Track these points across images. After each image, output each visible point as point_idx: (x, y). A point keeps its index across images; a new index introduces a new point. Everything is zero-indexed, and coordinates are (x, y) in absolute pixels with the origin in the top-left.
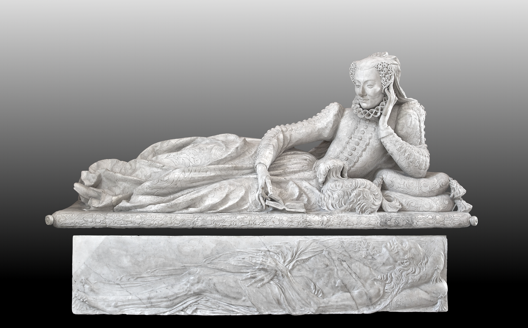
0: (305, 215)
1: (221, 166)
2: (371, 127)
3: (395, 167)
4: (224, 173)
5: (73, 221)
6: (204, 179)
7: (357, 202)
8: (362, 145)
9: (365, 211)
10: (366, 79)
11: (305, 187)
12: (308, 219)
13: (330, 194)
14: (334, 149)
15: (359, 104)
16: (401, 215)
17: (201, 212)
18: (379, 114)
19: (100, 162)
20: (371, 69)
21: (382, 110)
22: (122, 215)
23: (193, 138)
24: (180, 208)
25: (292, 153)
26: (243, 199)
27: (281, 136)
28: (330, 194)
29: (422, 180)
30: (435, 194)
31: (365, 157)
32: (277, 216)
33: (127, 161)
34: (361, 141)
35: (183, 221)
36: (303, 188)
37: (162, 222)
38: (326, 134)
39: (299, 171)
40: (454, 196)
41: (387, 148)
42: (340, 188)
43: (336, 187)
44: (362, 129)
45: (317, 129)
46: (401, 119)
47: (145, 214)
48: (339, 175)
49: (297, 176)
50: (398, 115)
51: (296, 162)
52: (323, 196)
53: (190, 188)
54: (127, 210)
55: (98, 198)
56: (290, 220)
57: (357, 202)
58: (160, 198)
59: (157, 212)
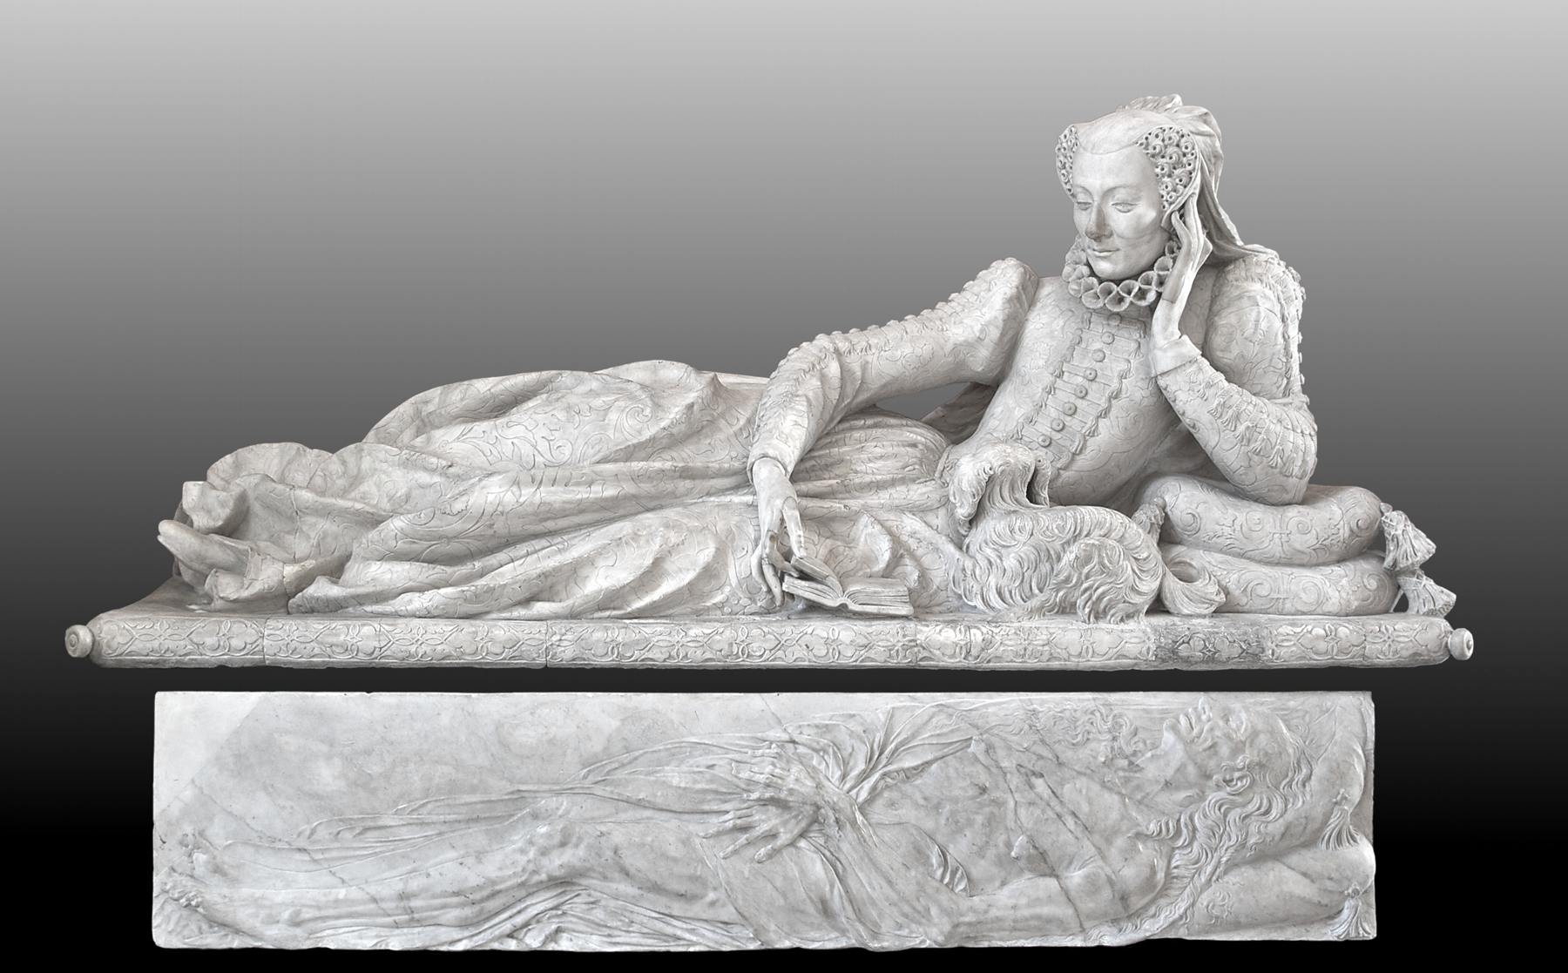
1: (636, 466)
2: (1127, 340)
4: (647, 487)
5: (156, 644)
6: (581, 508)
7: (1079, 583)
8: (1098, 397)
9: (1105, 612)
10: (1110, 182)
11: (913, 535)
12: (921, 638)
14: (1005, 409)
16: (1223, 625)
17: (574, 615)
18: (1151, 296)
19: (245, 453)
22: (316, 626)
23: (545, 374)
24: (505, 601)
25: (870, 422)
30: (1335, 557)
32: (819, 628)
33: (333, 448)
34: (1094, 386)
35: (515, 643)
36: (904, 538)
38: (980, 362)
39: (893, 483)
40: (1395, 563)
41: (1178, 407)
43: (1013, 534)
44: (1097, 345)
45: (949, 347)
46: (1224, 313)
47: (390, 621)
49: (884, 497)
51: (881, 451)
52: (968, 564)
53: (536, 536)
54: (332, 608)
55: (236, 569)
58: (439, 568)
59: (428, 615)
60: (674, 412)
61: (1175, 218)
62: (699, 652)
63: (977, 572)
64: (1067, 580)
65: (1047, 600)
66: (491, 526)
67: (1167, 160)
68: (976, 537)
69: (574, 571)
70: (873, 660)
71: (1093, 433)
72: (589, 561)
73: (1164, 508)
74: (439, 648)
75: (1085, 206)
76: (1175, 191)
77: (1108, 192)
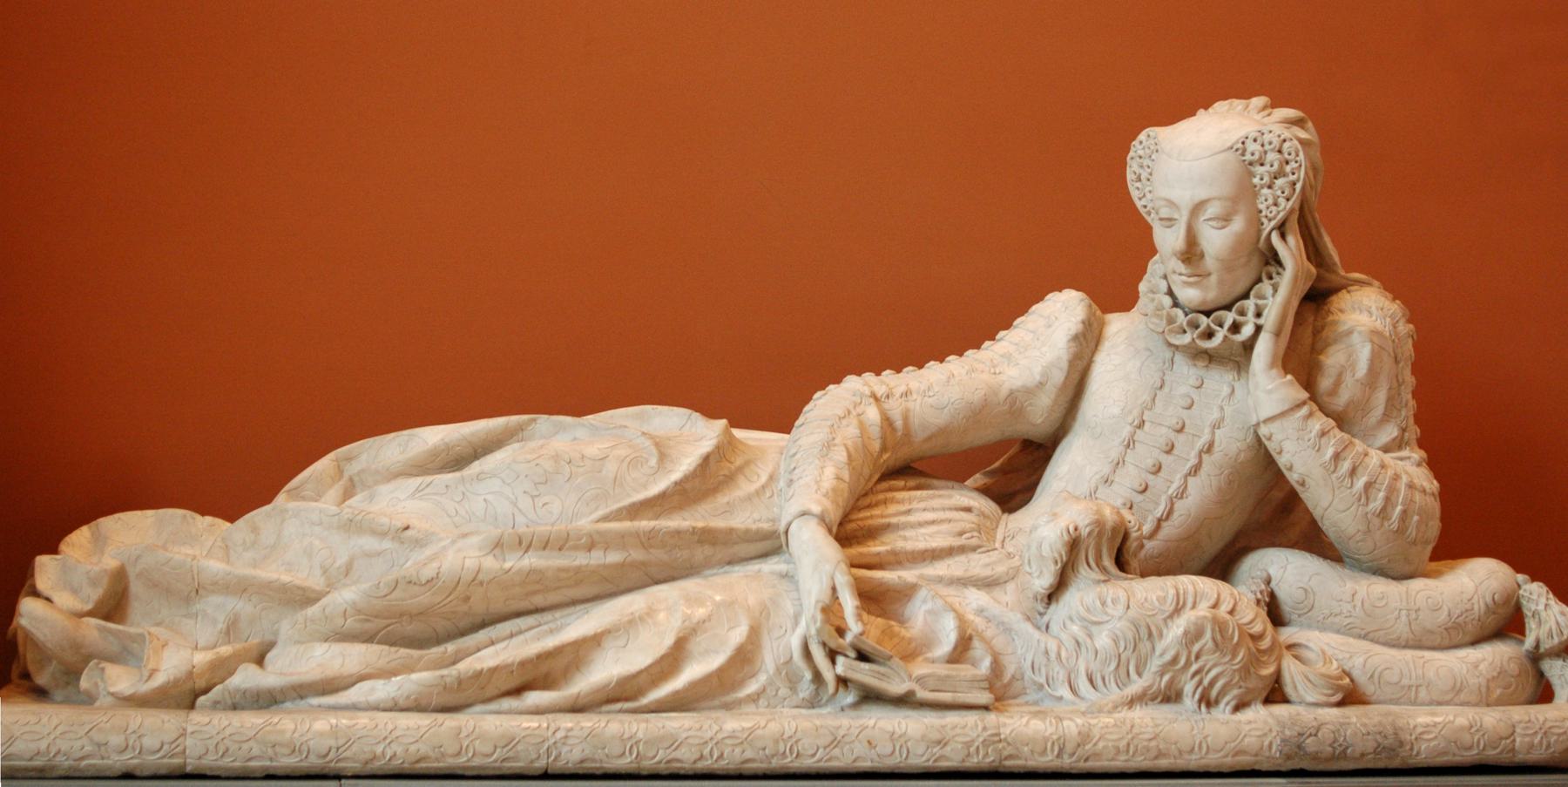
0: (991, 718)
1: (645, 524)
2: (1219, 380)
3: (1314, 541)
4: (658, 555)
5: (43, 745)
6: (578, 576)
7: (1188, 664)
8: (1187, 453)
9: (1217, 702)
10: (1202, 194)
11: (980, 611)
12: (1005, 732)
13: (1081, 636)
14: (1070, 469)
15: (1170, 293)
16: (1352, 713)
17: (577, 708)
18: (1247, 331)
19: (108, 523)
20: (1223, 156)
21: (1258, 315)
22: (251, 720)
23: (514, 419)
24: (491, 690)
25: (912, 483)
26: (744, 659)
27: (872, 414)
28: (1081, 636)
29: (1417, 584)
30: (1468, 638)
31: (1192, 496)
32: (883, 723)
33: (232, 518)
34: (1181, 437)
35: (510, 741)
36: (971, 617)
37: (424, 748)
38: (1039, 416)
39: (950, 552)
40: (1537, 646)
41: (1282, 461)
42: (1121, 608)
43: (1107, 605)
44: (1183, 389)
45: (1004, 392)
46: (1331, 350)
47: (347, 714)
48: (1108, 563)
49: (941, 569)
50: (1317, 332)
51: (932, 516)
52: (1052, 646)
53: (519, 614)
54: (267, 700)
55: (123, 655)
56: (936, 736)
57: (1188, 664)
58: (403, 651)
59: (395, 707)
60: (685, 464)
61: (1275, 238)
62: (738, 750)
63: (1063, 654)
64: (1175, 660)
65: (1150, 687)
66: (467, 599)
67: (1267, 167)
68: (1059, 611)
69: (577, 654)
70: (947, 759)
71: (1182, 494)
72: (594, 642)
73: (1268, 582)
74: (413, 748)
75: (1169, 222)
76: (1276, 204)
77: (1198, 208)
